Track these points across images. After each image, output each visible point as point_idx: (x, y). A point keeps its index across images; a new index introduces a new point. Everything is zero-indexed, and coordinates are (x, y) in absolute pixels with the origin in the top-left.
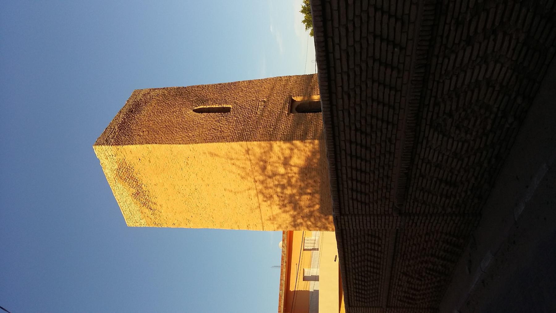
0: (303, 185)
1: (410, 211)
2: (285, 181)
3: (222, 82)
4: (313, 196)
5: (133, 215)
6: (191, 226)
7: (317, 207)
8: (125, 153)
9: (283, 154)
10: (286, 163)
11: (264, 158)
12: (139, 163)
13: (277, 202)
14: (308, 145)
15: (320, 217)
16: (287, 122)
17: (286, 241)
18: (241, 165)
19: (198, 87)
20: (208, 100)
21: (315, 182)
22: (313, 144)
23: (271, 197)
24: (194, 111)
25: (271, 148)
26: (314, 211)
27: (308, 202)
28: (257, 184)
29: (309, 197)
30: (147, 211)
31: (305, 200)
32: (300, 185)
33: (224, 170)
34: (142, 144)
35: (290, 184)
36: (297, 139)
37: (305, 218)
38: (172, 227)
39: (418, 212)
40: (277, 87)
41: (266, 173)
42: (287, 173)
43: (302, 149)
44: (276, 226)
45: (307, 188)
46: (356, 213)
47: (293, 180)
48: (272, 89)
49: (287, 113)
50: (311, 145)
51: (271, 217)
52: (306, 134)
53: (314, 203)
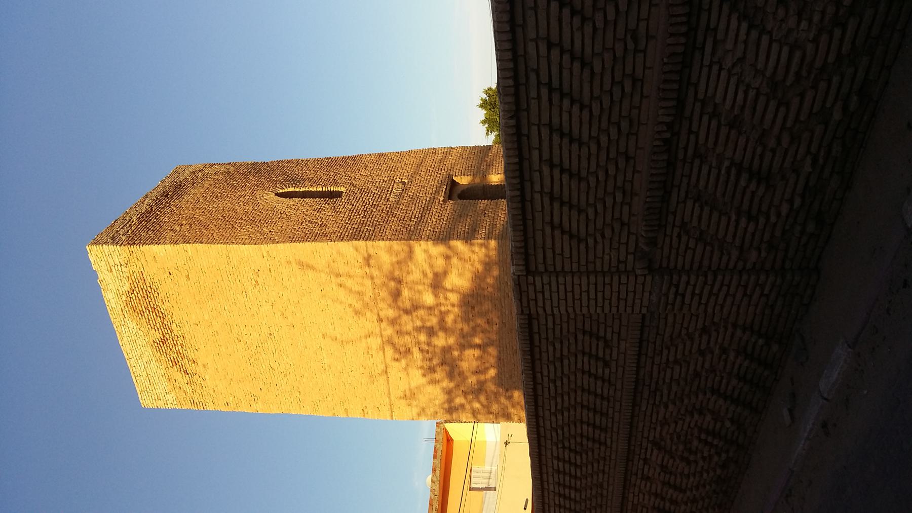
0: (466, 328)
1: (672, 265)
2: (433, 321)
3: (333, 155)
4: (484, 352)
5: (155, 386)
6: (259, 408)
7: (492, 372)
8: (143, 261)
9: (431, 266)
10: (437, 285)
11: (397, 273)
12: (169, 281)
13: (419, 363)
14: (477, 249)
15: (496, 394)
16: (443, 212)
17: (438, 472)
18: (356, 288)
19: (289, 162)
20: (304, 180)
21: (488, 323)
22: (487, 247)
23: (408, 351)
24: (277, 194)
25: (411, 252)
26: (486, 381)
27: (475, 364)
28: (384, 325)
29: (477, 352)
30: (178, 376)
31: (469, 359)
32: (462, 329)
33: (324, 296)
34: (176, 243)
35: (443, 327)
36: (458, 238)
37: (468, 397)
38: (224, 409)
39: (687, 267)
40: (428, 162)
41: (400, 304)
42: (439, 305)
43: (467, 257)
44: (415, 411)
45: (473, 335)
46: (559, 269)
47: (450, 319)
48: (419, 165)
49: (442, 199)
50: (483, 250)
51: (408, 393)
52: (475, 230)
53: (487, 365)
